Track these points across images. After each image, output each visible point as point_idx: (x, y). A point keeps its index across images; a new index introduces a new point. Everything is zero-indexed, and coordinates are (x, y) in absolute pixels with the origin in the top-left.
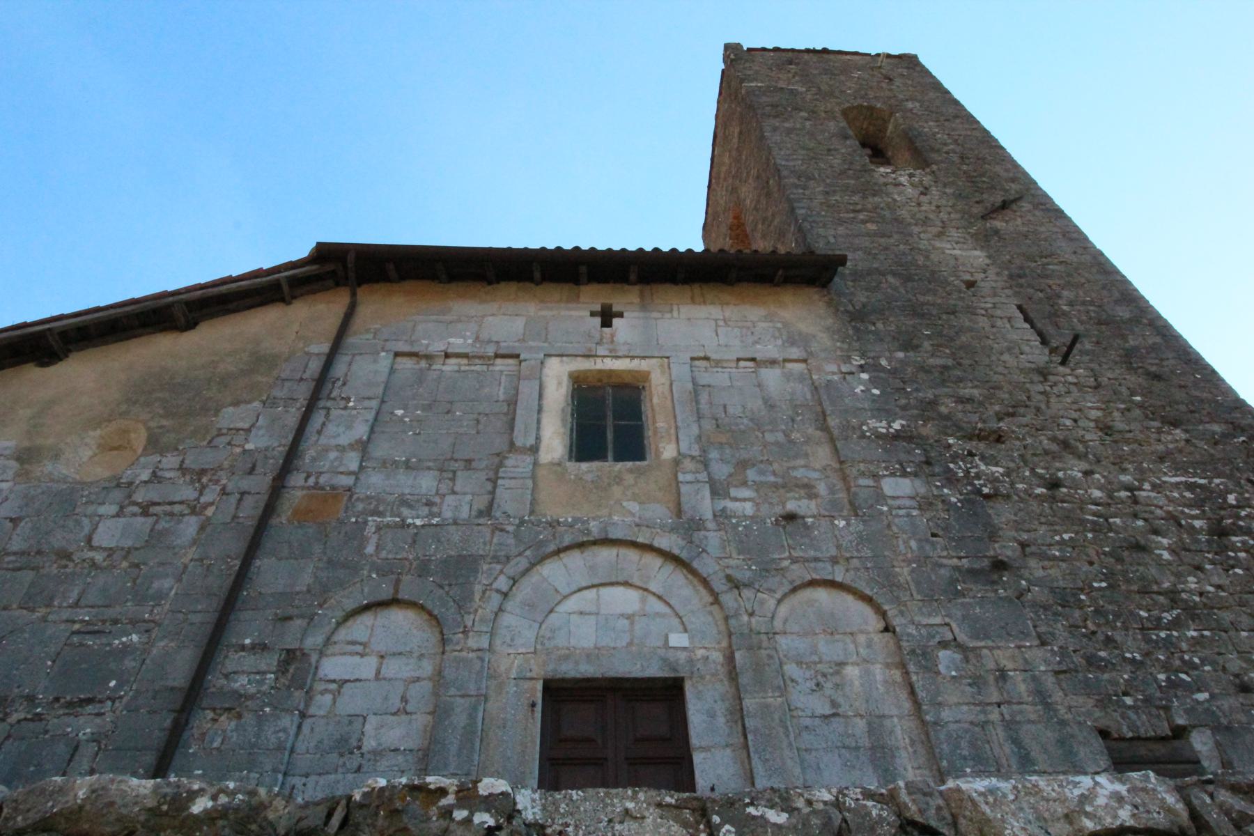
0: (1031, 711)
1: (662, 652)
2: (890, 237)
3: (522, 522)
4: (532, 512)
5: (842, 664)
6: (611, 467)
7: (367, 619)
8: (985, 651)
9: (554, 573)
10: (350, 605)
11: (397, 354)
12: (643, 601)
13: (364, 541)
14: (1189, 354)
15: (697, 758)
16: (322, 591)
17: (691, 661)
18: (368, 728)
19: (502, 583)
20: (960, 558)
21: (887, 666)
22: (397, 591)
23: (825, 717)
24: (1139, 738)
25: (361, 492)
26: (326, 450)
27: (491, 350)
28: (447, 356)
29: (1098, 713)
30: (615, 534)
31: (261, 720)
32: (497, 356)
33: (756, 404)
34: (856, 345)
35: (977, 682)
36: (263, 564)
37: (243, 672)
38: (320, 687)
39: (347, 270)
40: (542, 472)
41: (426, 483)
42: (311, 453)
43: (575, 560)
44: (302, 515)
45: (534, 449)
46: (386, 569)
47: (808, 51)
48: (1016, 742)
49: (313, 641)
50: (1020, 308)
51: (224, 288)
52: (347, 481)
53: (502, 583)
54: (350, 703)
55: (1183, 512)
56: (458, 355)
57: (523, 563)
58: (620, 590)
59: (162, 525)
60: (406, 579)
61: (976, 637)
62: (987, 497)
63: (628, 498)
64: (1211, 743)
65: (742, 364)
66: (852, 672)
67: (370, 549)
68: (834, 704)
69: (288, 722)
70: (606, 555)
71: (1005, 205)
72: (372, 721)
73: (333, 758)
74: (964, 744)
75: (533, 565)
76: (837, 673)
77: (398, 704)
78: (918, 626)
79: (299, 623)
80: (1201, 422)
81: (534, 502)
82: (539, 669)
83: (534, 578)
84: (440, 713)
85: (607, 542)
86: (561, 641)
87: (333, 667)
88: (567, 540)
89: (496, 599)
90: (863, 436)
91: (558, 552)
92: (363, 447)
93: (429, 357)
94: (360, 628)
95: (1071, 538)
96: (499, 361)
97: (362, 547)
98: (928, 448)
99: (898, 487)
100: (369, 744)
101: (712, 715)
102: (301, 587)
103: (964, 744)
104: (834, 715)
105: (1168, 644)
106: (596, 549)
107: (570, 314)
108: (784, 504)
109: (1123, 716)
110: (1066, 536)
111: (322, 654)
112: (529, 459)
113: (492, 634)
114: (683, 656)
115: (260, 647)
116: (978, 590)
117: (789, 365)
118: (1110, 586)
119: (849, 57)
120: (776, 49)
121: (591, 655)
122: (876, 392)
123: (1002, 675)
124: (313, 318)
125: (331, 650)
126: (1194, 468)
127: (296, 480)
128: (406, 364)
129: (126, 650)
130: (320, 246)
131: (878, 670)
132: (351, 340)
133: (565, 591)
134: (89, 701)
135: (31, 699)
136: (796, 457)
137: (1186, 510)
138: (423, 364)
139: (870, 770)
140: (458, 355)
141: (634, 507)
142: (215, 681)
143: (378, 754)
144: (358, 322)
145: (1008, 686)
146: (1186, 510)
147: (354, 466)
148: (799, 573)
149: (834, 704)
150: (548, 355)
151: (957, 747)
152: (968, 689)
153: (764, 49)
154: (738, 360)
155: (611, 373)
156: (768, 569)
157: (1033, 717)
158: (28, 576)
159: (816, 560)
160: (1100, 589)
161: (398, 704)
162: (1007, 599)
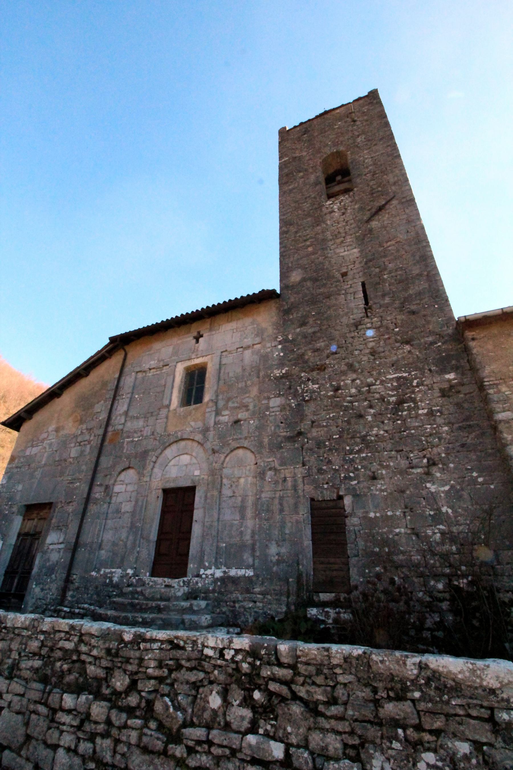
0: (290, 493)
1: (192, 477)
2: (317, 253)
3: (161, 435)
4: (165, 431)
5: (239, 478)
6: (193, 406)
7: (124, 473)
8: (283, 471)
9: (169, 452)
10: (119, 470)
11: (137, 372)
12: (191, 459)
13: (123, 448)
14: (438, 290)
15: (195, 511)
16: (114, 466)
17: (199, 480)
18: (123, 506)
19: (154, 459)
20: (287, 432)
21: (253, 477)
22: (130, 464)
23: (230, 497)
24: (324, 500)
25: (125, 429)
26: (117, 417)
27: (161, 364)
28: (150, 369)
29: (313, 492)
30: (185, 436)
31: (101, 505)
32: (164, 366)
33: (239, 370)
34: (282, 329)
35: (276, 483)
36: (103, 459)
37: (98, 493)
38: (114, 494)
39: (121, 343)
40: (171, 414)
41: (141, 423)
42: (114, 418)
43: (174, 447)
44: (111, 441)
45: (168, 406)
46: (128, 457)
47: (317, 117)
48: (281, 504)
49: (112, 482)
50: (363, 285)
51: (93, 359)
52: (121, 427)
53: (154, 459)
54: (120, 499)
55: (388, 394)
56: (154, 368)
57: (159, 451)
58: (185, 456)
59: (83, 448)
60: (132, 460)
61: (281, 465)
62: (307, 401)
63: (196, 418)
64: (350, 501)
65: (239, 350)
66: (242, 480)
67: (125, 451)
68: (234, 492)
69: (105, 506)
70: (183, 443)
71: (381, 209)
72: (124, 504)
73: (115, 515)
74: (265, 506)
75: (162, 451)
76: (238, 481)
77: (129, 499)
78: (264, 461)
79: (109, 477)
80: (424, 337)
81: (166, 427)
82: (161, 485)
83: (163, 455)
84: (137, 501)
85: (182, 439)
86: (167, 476)
87: (117, 488)
88: (172, 441)
89: (152, 464)
90: (270, 380)
91: (169, 445)
92: (126, 413)
93: (144, 372)
94: (122, 476)
95: (333, 416)
96: (165, 368)
97: (123, 450)
98: (292, 380)
99: (276, 402)
100: (123, 511)
101: (201, 498)
102: (109, 466)
103: (265, 506)
104: (233, 496)
105: (352, 461)
106: (180, 442)
107: (184, 341)
108: (237, 415)
109: (322, 492)
110: (331, 415)
111: (114, 485)
112: (166, 410)
113: (151, 476)
114: (197, 478)
115: (101, 485)
116: (289, 445)
117: (255, 346)
118: (340, 437)
119: (338, 111)
120: (301, 124)
121: (175, 479)
122: (282, 354)
123: (285, 480)
124: (114, 363)
125: (117, 483)
126: (405, 368)
127: (110, 429)
128: (140, 375)
129: (76, 488)
130: (110, 339)
131: (250, 479)
132: (126, 369)
133: (170, 458)
134: (71, 502)
135: (61, 502)
136: (246, 393)
137: (390, 393)
138: (144, 374)
139: (238, 514)
140: (154, 368)
141: (193, 424)
142: (93, 495)
143: (124, 513)
144: (128, 361)
145: (286, 484)
146: (390, 393)
147: (123, 421)
148: (234, 444)
149: (234, 492)
150: (177, 362)
151: (263, 506)
152: (273, 485)
153: (295, 127)
154: (237, 349)
155: (197, 365)
156: (225, 444)
157: (290, 495)
158: (59, 467)
159: (240, 439)
160: (336, 438)
161: (129, 499)
162: (297, 449)
